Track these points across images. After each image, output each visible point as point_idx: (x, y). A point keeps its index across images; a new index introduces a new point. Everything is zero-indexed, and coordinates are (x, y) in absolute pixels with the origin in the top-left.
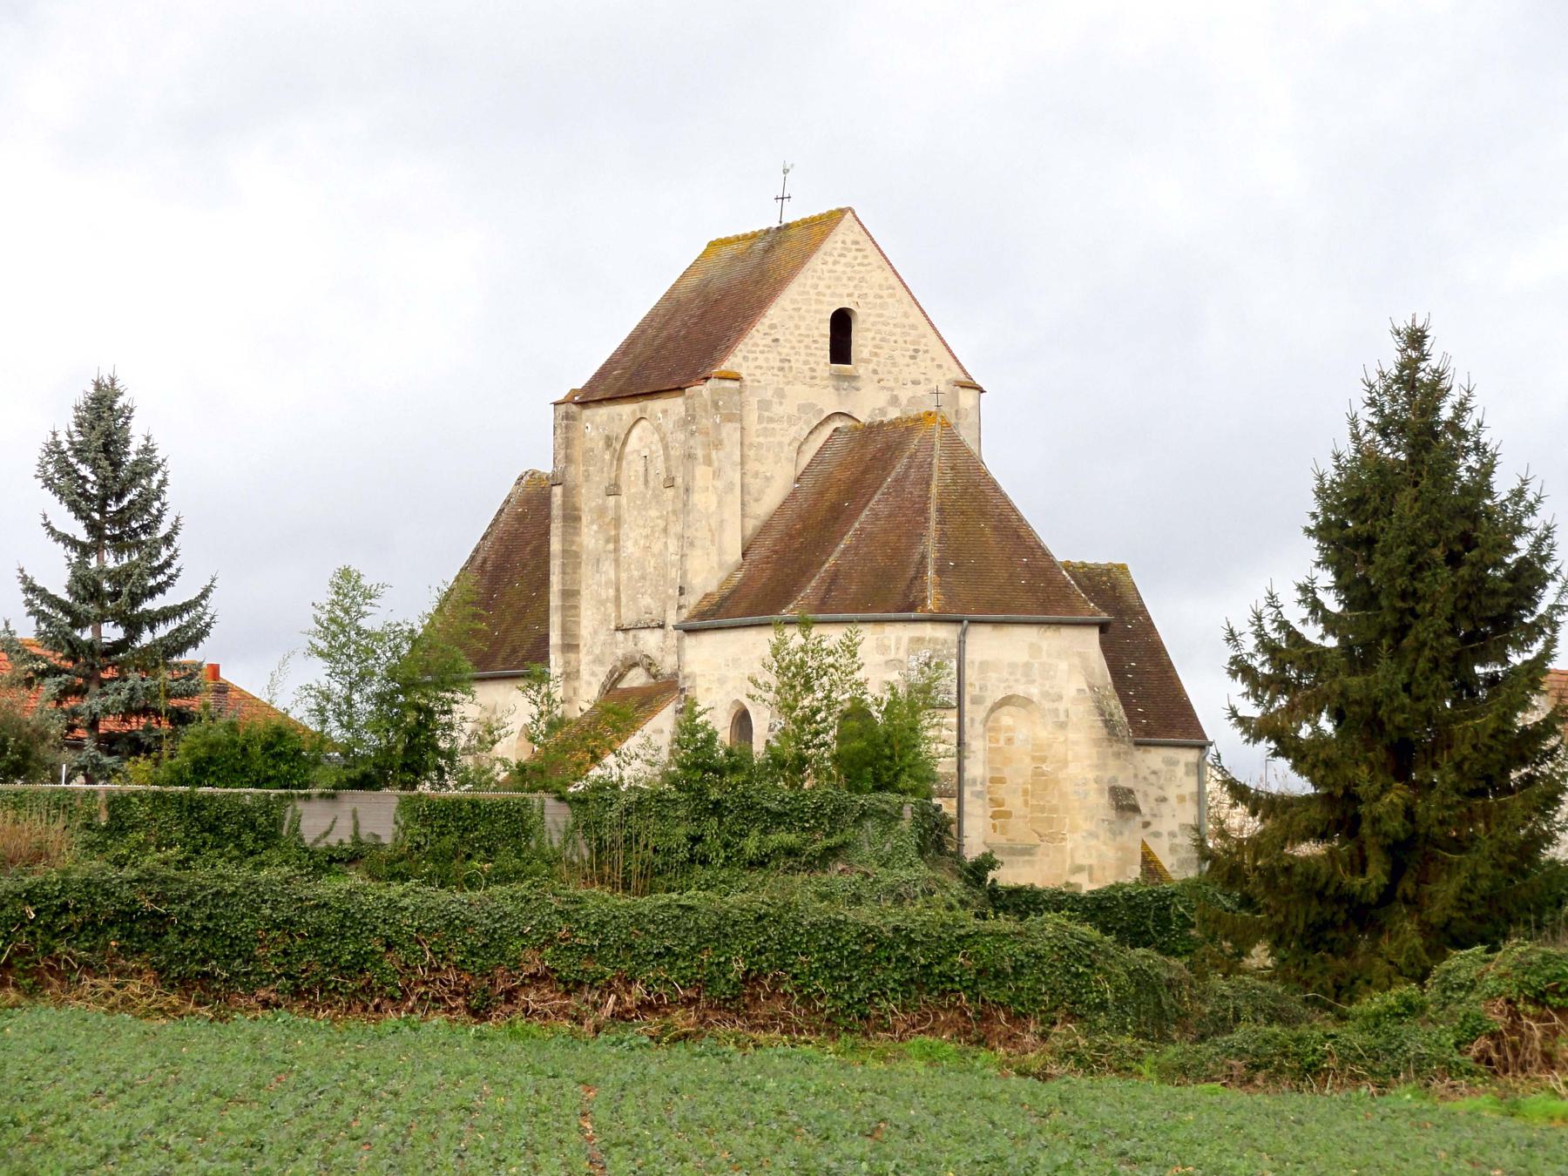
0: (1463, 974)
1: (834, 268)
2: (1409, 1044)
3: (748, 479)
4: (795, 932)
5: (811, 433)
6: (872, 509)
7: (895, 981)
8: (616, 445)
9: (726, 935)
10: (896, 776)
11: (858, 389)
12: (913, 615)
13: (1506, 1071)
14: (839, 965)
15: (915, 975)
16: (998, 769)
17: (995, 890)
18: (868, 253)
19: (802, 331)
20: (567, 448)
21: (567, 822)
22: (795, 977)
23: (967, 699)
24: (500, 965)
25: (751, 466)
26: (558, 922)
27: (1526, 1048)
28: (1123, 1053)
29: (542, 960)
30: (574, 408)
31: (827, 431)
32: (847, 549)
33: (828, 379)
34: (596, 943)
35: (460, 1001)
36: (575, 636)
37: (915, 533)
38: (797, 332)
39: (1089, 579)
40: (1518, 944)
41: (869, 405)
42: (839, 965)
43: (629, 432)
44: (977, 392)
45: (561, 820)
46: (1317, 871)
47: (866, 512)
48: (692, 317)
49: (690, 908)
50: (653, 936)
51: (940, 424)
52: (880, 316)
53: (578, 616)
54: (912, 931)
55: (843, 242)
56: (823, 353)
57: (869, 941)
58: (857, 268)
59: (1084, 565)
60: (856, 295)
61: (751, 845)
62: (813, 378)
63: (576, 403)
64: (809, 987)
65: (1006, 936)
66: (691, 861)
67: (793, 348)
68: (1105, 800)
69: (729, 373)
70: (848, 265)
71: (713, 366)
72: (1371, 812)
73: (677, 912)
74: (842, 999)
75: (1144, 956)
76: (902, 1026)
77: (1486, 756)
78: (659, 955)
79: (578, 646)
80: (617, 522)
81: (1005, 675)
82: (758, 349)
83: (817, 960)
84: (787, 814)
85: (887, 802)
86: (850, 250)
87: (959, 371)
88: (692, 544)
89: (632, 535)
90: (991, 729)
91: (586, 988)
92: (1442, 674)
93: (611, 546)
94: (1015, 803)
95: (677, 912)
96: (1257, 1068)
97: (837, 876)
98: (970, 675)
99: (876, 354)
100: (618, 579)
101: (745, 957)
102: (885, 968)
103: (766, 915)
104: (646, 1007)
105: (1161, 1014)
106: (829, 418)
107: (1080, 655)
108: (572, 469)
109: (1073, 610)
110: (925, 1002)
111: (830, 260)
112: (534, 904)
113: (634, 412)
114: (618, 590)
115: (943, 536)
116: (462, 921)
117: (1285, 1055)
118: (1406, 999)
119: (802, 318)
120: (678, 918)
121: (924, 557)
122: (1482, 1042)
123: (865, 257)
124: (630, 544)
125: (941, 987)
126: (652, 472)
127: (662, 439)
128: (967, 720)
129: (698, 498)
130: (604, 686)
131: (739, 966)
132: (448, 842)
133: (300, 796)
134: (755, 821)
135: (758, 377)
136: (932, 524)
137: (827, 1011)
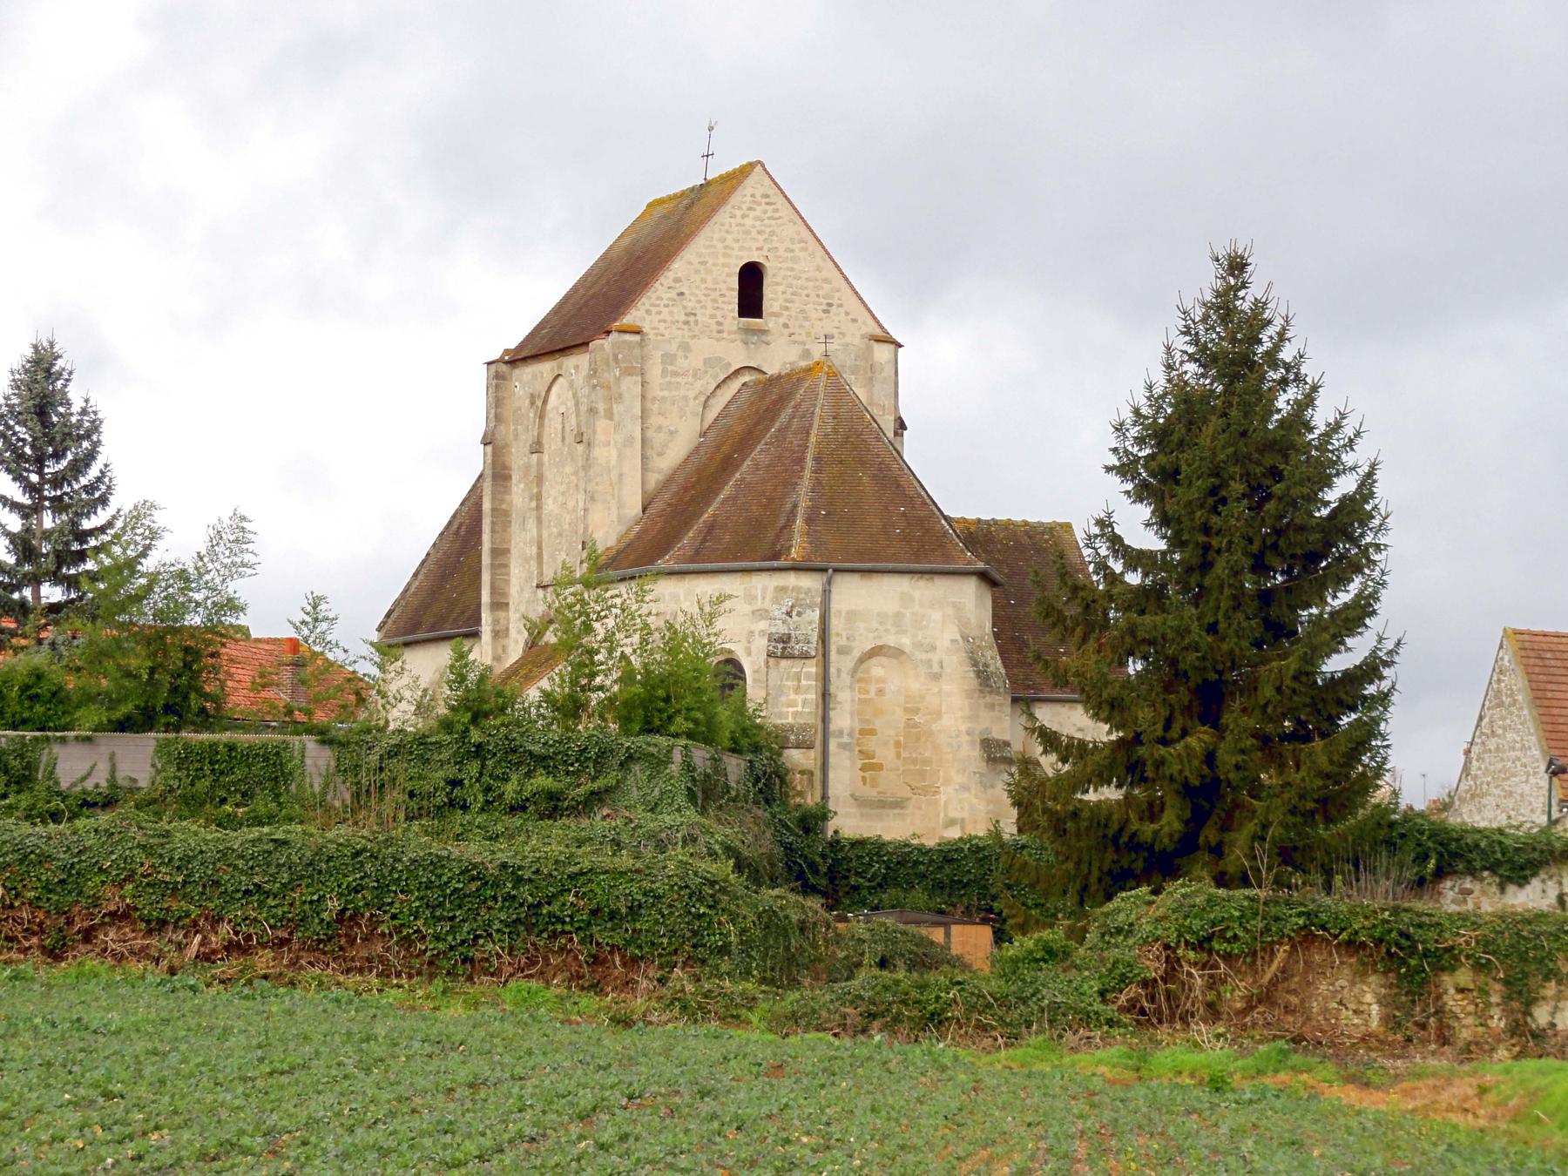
0: (1122, 917)
1: (742, 222)
2: (1044, 992)
3: (650, 433)
4: (394, 868)
5: (718, 386)
6: (753, 459)
7: (501, 921)
8: (540, 403)
9: (320, 872)
10: (670, 718)
11: (768, 344)
12: (775, 564)
13: (1160, 1022)
14: (441, 905)
15: (523, 915)
16: (867, 721)
17: (838, 842)
18: (778, 206)
19: (710, 284)
20: (497, 407)
21: (328, 765)
22: (394, 917)
23: (833, 649)
24: (77, 902)
25: (654, 420)
26: (140, 856)
27: (1187, 998)
28: (732, 1000)
29: (123, 898)
30: (504, 368)
31: (735, 385)
32: (725, 500)
33: (735, 333)
34: (180, 879)
35: (35, 940)
36: (505, 595)
37: (790, 484)
38: (704, 286)
39: (1030, 537)
40: (1182, 886)
41: (777, 358)
42: (441, 905)
43: (549, 389)
44: (892, 346)
45: (322, 763)
46: (1109, 818)
47: (748, 462)
48: (615, 275)
49: (285, 843)
50: (242, 872)
51: (828, 373)
52: (792, 269)
53: (508, 574)
54: (520, 868)
55: (753, 196)
56: (730, 307)
57: (473, 879)
58: (767, 222)
59: (1026, 523)
60: (766, 247)
61: (510, 789)
62: (720, 332)
63: (507, 363)
64: (409, 927)
65: (622, 874)
66: (451, 804)
67: (699, 302)
68: (977, 752)
69: (629, 326)
70: (756, 218)
71: (615, 320)
72: (1152, 755)
73: (271, 846)
74: (445, 940)
75: (777, 897)
76: (508, 970)
77: (1291, 699)
78: (247, 892)
79: (507, 604)
80: (540, 479)
81: (875, 625)
82: (662, 303)
83: (418, 899)
84: (551, 758)
85: (655, 745)
86: (759, 204)
87: (875, 325)
88: (592, 498)
89: (553, 492)
90: (860, 681)
91: (171, 927)
92: (1244, 612)
93: (534, 504)
94: (885, 755)
95: (271, 846)
96: (872, 1016)
97: (599, 823)
98: (836, 624)
99: (787, 308)
100: (540, 536)
101: (340, 895)
102: (490, 908)
103: (364, 850)
104: (230, 947)
105: (791, 959)
106: (737, 372)
107: (954, 605)
108: (502, 428)
109: (948, 558)
110: (533, 944)
111: (738, 213)
112: (116, 838)
113: (552, 370)
114: (540, 548)
115: (817, 484)
116: (37, 855)
117: (904, 1002)
118: (1047, 942)
119: (709, 272)
120: (270, 853)
121: (795, 506)
122: (1133, 991)
123: (777, 210)
124: (550, 501)
125: (551, 928)
126: (568, 429)
127: (575, 395)
128: (833, 670)
129: (597, 452)
130: (526, 643)
131: (334, 905)
132: (203, 785)
133: (57, 738)
134: (519, 764)
135: (662, 331)
136: (807, 474)
137: (428, 954)
